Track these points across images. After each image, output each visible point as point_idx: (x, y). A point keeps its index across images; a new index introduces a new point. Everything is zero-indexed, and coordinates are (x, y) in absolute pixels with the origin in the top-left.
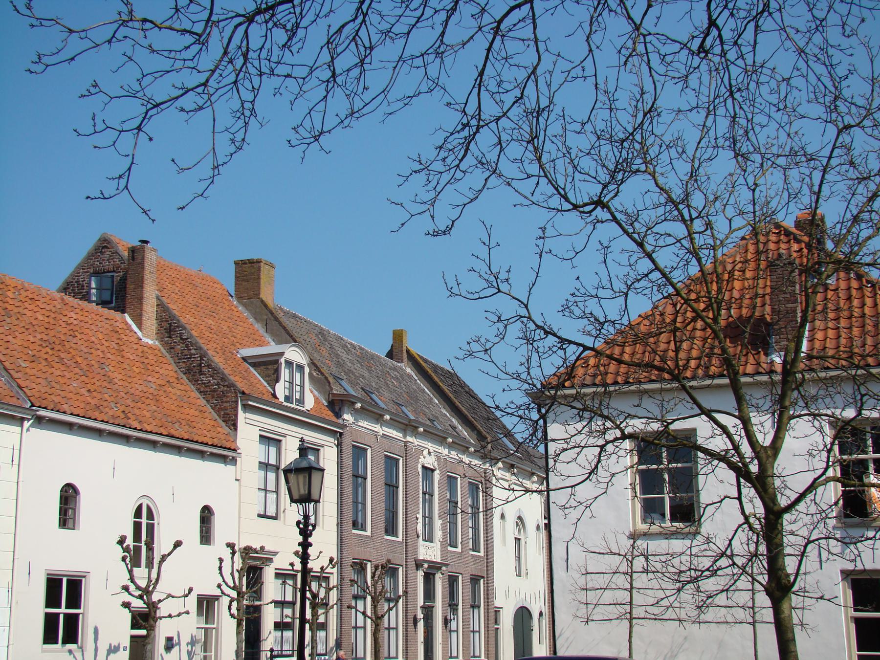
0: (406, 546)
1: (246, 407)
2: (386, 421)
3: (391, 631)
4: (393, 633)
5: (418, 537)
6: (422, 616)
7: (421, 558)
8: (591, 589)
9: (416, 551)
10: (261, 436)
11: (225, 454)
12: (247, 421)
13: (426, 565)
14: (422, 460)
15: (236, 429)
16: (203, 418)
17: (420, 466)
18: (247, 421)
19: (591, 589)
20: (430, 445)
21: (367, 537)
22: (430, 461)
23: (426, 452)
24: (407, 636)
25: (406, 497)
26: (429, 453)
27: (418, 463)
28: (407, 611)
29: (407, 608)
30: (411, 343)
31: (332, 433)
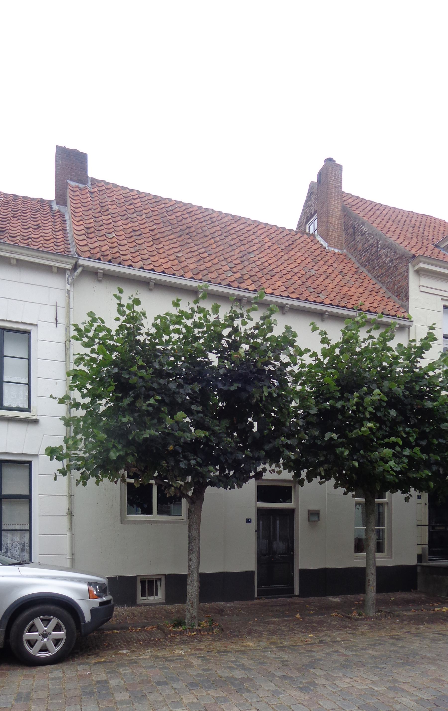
1: (419, 272)
15: (408, 299)
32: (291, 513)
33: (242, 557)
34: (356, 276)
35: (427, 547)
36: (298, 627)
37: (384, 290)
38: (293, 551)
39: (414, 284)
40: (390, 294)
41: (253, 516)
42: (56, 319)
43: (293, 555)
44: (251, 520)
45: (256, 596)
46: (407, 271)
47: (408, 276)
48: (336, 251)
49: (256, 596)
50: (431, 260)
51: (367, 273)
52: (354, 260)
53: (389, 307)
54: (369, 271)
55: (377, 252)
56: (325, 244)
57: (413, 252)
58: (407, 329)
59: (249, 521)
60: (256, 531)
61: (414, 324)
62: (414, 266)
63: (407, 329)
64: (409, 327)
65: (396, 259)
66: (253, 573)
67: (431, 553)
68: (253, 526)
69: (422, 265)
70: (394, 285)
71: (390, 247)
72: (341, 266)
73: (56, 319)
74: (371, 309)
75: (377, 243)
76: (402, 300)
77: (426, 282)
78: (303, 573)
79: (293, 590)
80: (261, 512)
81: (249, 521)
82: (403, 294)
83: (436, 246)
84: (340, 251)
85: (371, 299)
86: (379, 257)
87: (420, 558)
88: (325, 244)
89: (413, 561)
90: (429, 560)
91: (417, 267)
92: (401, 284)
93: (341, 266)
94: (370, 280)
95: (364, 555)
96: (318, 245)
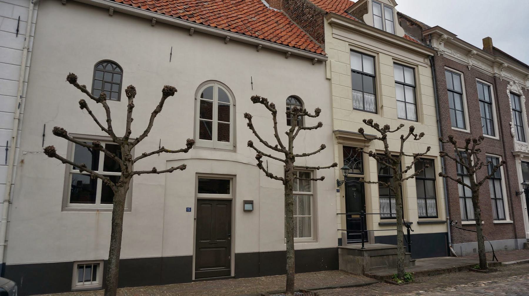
0: (503, 143)
1: (331, 24)
2: (473, 54)
3: (498, 202)
4: (499, 203)
5: (512, 137)
6: (523, 190)
7: (517, 150)
8: (391, 212)
9: (512, 147)
10: (351, 50)
11: (316, 59)
12: (334, 36)
13: (522, 156)
14: (509, 87)
15: (324, 42)
16: (292, 35)
17: (508, 91)
18: (334, 36)
19: (391, 212)
20: (516, 79)
21: (467, 133)
22: (516, 89)
23: (511, 83)
24: (512, 204)
25: (499, 110)
26: (514, 83)
27: (509, 109)
28: (509, 187)
29: (509, 184)
30: (496, 44)
31: (427, 56)
32: (229, 202)
33: (182, 243)
34: (288, 26)
35: (346, 232)
36: (521, 278)
37: (308, 35)
38: (230, 236)
39: (328, 31)
40: (312, 39)
41: (192, 204)
42: (18, 30)
43: (230, 240)
44: (190, 209)
45: (194, 279)
46: (323, 23)
47: (323, 26)
48: (276, 10)
49: (194, 279)
50: (340, 17)
51: (296, 24)
52: (287, 16)
53: (310, 47)
54: (298, 24)
55: (303, 10)
56: (267, 5)
57: (327, 11)
58: (324, 62)
59: (188, 210)
60: (195, 219)
61: (329, 59)
62: (327, 20)
63: (324, 62)
64: (325, 61)
65: (316, 15)
66: (191, 257)
67: (349, 237)
68: (192, 215)
69: (333, 19)
70: (315, 32)
71: (311, 7)
72: (278, 19)
73: (18, 30)
74: (296, 46)
75: (303, 5)
76: (320, 42)
77: (336, 31)
78: (238, 256)
79: (229, 272)
80: (200, 201)
81: (188, 210)
82: (321, 39)
83: (345, 12)
84: (279, 11)
85: (297, 40)
86: (304, 14)
87: (340, 241)
88: (267, 5)
89: (334, 244)
90: (348, 243)
91: (329, 21)
92: (319, 32)
93: (278, 19)
94: (298, 28)
95: (111, 206)
96: (262, 5)
